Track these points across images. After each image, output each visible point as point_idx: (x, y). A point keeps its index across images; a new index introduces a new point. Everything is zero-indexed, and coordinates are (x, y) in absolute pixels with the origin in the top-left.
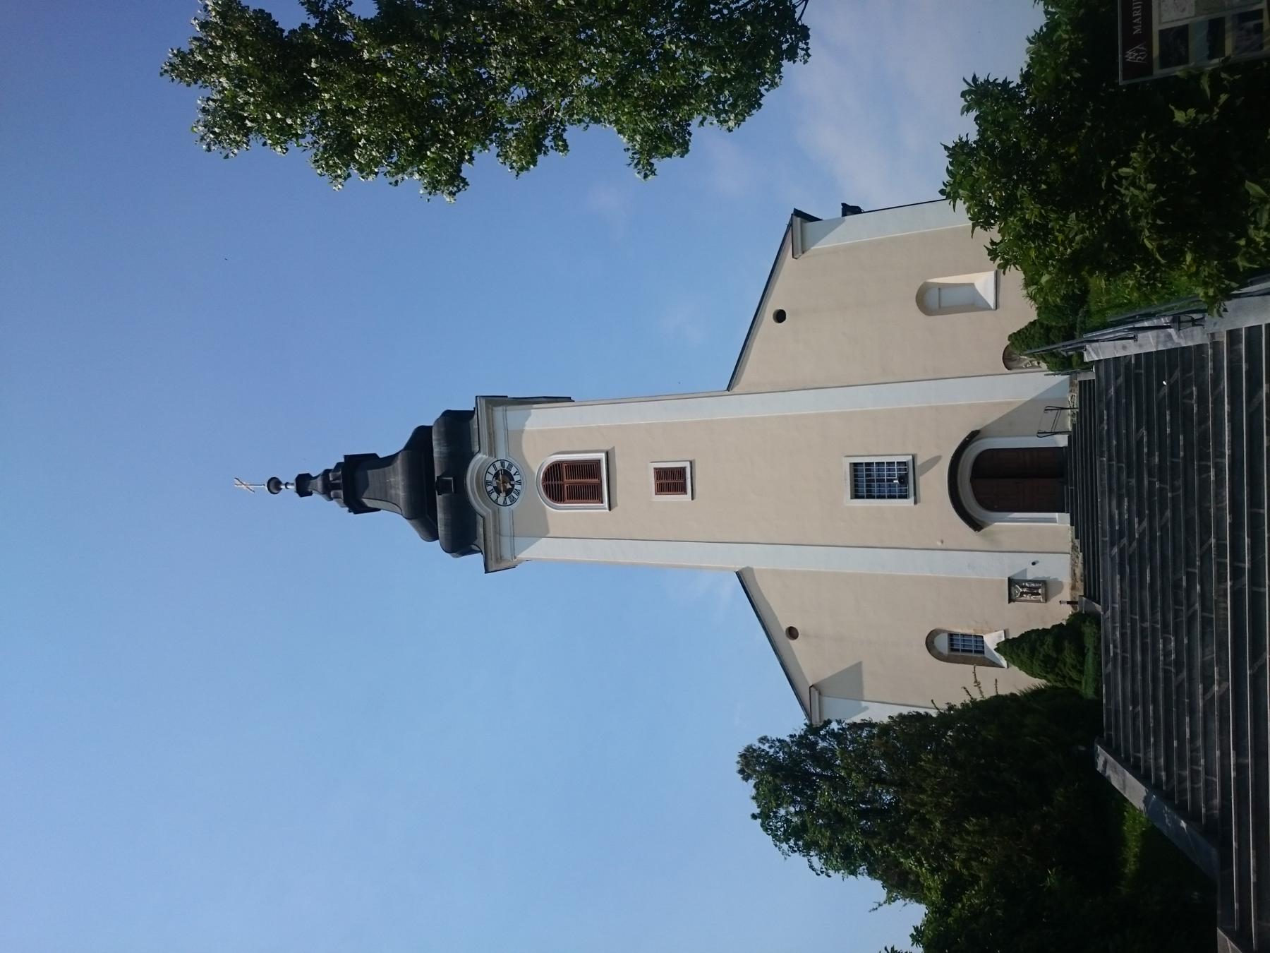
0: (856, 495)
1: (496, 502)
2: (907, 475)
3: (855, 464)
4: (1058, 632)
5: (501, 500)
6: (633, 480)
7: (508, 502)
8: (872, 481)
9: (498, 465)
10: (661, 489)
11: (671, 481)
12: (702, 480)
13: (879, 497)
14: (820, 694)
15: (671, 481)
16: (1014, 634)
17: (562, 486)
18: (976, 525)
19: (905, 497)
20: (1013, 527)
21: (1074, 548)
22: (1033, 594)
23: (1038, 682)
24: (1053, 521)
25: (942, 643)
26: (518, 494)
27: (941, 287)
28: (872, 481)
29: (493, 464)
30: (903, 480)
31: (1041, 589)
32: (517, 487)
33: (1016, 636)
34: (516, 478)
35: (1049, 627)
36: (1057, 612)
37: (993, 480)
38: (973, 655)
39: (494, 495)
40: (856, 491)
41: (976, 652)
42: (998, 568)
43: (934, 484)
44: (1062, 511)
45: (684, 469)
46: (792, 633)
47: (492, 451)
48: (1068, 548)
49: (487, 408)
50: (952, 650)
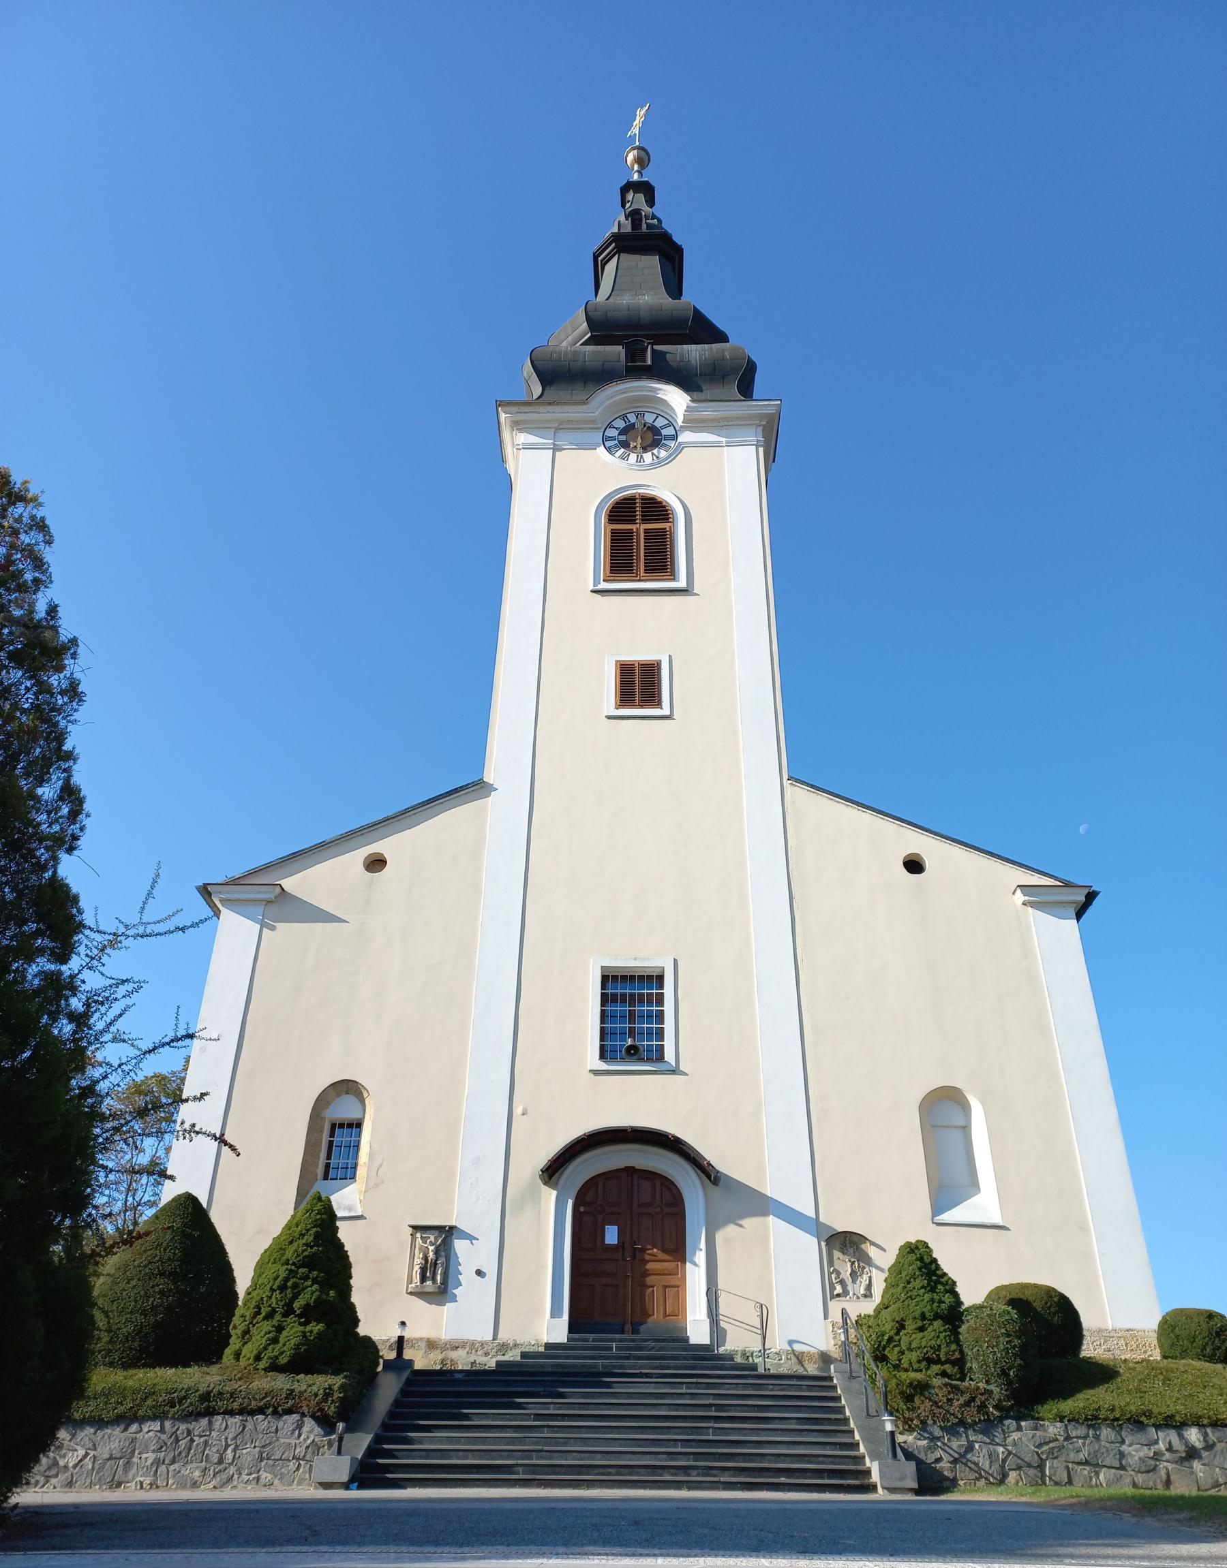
0: (609, 978)
1: (609, 426)
2: (641, 1060)
3: (660, 979)
4: (342, 1314)
5: (612, 433)
6: (642, 624)
7: (608, 444)
8: (631, 1013)
9: (668, 431)
10: (626, 671)
11: (639, 685)
12: (640, 731)
13: (603, 1013)
14: (269, 902)
15: (639, 685)
16: (345, 1233)
17: (633, 521)
18: (552, 1171)
19: (603, 1056)
20: (545, 1225)
21: (504, 1348)
22: (423, 1270)
23: (243, 1280)
24: (555, 1313)
25: (344, 1110)
26: (622, 457)
27: (966, 1129)
28: (631, 1013)
29: (670, 424)
30: (633, 1053)
31: (437, 1274)
32: (633, 457)
33: (342, 1235)
34: (648, 457)
35: (355, 1298)
36: (385, 1309)
37: (629, 1204)
38: (322, 1161)
39: (621, 424)
40: (615, 978)
41: (327, 1166)
42: (471, 1206)
43: (634, 1101)
44: (572, 1329)
45: (659, 704)
46: (376, 863)
47: (693, 424)
48: (503, 1336)
49: (761, 417)
50: (333, 1126)
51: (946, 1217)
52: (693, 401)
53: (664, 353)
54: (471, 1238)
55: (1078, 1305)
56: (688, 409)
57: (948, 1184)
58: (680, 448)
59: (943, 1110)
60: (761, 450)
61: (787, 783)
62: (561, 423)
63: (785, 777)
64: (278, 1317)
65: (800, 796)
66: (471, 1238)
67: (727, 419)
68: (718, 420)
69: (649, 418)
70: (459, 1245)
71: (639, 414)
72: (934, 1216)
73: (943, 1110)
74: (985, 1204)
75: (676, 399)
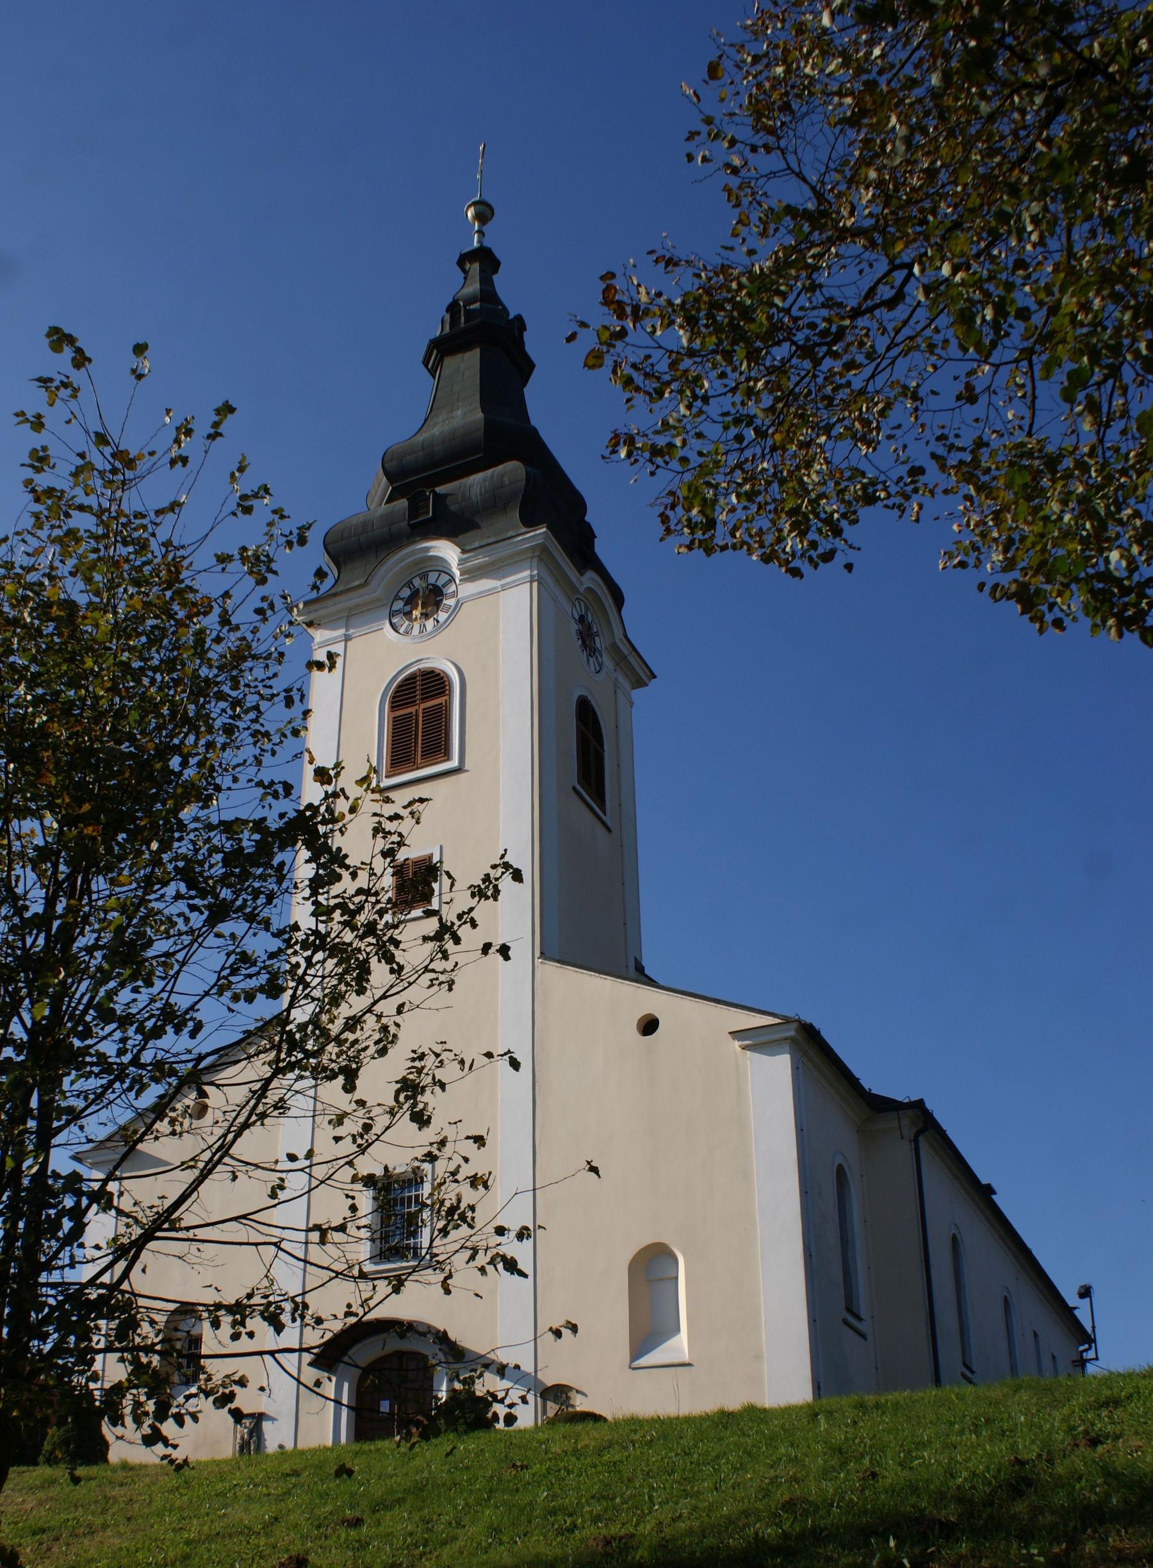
1: (397, 598)
17: (413, 703)
34: (430, 624)
39: (406, 593)
47: (471, 574)
49: (532, 548)
51: (643, 1361)
52: (464, 551)
53: (445, 496)
54: (273, 1419)
55: (817, 1026)
56: (461, 562)
57: (648, 1329)
58: (459, 605)
59: (651, 1268)
60: (535, 585)
61: (538, 961)
62: (350, 609)
63: (537, 954)
64: (729, 419)
65: (551, 971)
66: (273, 1419)
67: (501, 560)
68: (493, 563)
69: (432, 578)
70: (266, 1426)
71: (424, 576)
72: (632, 1361)
73: (651, 1268)
74: (680, 1346)
75: (447, 551)
